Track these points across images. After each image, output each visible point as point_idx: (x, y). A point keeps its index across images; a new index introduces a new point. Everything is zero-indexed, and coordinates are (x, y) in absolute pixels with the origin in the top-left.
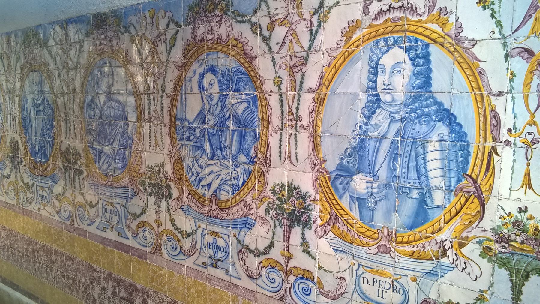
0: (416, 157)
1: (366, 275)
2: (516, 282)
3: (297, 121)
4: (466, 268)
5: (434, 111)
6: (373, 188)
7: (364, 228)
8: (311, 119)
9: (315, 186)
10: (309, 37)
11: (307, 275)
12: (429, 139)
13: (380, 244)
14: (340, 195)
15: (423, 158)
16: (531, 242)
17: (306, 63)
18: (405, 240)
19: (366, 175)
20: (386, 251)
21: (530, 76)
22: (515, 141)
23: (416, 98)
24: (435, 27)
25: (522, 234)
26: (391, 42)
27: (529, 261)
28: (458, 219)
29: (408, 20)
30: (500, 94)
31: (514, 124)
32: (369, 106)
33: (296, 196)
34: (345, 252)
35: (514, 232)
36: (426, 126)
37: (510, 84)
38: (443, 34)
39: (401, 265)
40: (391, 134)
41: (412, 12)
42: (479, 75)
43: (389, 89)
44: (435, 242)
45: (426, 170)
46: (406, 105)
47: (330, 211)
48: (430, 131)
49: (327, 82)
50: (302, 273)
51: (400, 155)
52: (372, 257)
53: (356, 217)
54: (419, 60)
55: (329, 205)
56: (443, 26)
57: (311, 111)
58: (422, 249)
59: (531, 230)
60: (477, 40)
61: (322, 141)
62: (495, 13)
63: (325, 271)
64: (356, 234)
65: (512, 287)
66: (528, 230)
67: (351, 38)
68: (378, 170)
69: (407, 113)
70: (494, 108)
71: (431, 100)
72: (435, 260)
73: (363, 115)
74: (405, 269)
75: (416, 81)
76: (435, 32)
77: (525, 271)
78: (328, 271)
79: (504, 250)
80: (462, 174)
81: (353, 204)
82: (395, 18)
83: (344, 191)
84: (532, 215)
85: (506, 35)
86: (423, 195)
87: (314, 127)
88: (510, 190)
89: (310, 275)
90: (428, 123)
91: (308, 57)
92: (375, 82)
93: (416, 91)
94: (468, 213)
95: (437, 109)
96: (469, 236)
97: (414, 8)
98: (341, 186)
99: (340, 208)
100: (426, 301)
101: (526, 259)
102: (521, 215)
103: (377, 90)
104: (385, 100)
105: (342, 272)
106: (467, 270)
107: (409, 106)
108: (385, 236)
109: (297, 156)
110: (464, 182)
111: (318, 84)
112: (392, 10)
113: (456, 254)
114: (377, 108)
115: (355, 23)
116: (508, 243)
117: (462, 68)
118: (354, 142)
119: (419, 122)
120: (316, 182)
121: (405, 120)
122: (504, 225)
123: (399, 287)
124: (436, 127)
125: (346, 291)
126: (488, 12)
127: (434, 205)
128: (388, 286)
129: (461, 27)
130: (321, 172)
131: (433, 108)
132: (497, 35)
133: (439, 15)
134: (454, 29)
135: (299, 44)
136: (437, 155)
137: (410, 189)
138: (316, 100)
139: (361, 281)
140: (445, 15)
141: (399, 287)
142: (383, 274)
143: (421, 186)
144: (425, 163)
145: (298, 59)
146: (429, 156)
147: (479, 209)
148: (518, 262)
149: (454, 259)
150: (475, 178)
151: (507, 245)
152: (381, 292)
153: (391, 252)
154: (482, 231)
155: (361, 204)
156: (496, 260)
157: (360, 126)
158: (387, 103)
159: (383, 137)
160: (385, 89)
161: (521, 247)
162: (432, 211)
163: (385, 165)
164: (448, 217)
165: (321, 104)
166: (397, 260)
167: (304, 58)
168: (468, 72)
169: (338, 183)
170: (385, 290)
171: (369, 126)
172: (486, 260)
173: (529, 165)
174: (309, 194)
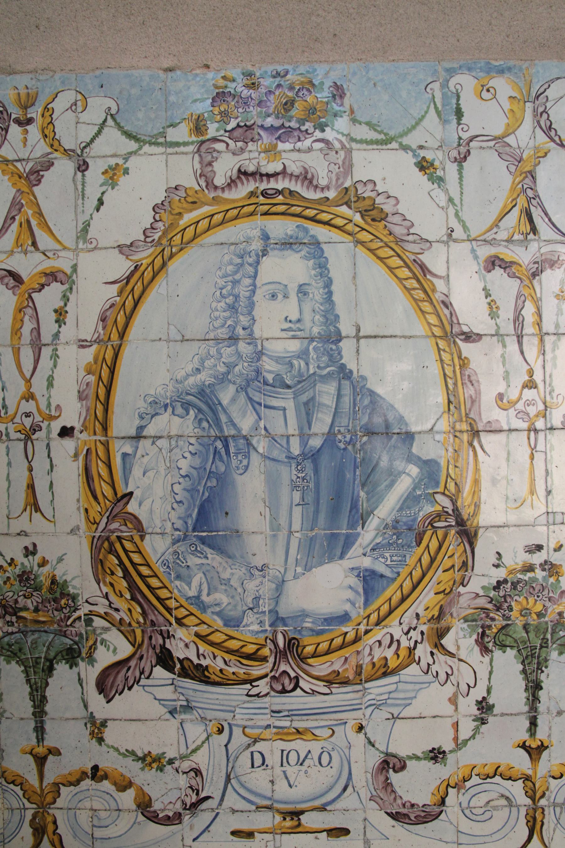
2: (36, 683)
16: (48, 605)
22: (6, 429)
25: (34, 594)
27: (50, 640)
35: (20, 594)
59: (47, 584)
65: (31, 694)
77: (46, 659)
79: (10, 629)
84: (44, 558)
88: (8, 518)
101: (44, 636)
102: (29, 560)
116: (15, 614)
122: (5, 583)
148: (34, 646)
151: (14, 619)
161: (35, 618)
173: (31, 470)
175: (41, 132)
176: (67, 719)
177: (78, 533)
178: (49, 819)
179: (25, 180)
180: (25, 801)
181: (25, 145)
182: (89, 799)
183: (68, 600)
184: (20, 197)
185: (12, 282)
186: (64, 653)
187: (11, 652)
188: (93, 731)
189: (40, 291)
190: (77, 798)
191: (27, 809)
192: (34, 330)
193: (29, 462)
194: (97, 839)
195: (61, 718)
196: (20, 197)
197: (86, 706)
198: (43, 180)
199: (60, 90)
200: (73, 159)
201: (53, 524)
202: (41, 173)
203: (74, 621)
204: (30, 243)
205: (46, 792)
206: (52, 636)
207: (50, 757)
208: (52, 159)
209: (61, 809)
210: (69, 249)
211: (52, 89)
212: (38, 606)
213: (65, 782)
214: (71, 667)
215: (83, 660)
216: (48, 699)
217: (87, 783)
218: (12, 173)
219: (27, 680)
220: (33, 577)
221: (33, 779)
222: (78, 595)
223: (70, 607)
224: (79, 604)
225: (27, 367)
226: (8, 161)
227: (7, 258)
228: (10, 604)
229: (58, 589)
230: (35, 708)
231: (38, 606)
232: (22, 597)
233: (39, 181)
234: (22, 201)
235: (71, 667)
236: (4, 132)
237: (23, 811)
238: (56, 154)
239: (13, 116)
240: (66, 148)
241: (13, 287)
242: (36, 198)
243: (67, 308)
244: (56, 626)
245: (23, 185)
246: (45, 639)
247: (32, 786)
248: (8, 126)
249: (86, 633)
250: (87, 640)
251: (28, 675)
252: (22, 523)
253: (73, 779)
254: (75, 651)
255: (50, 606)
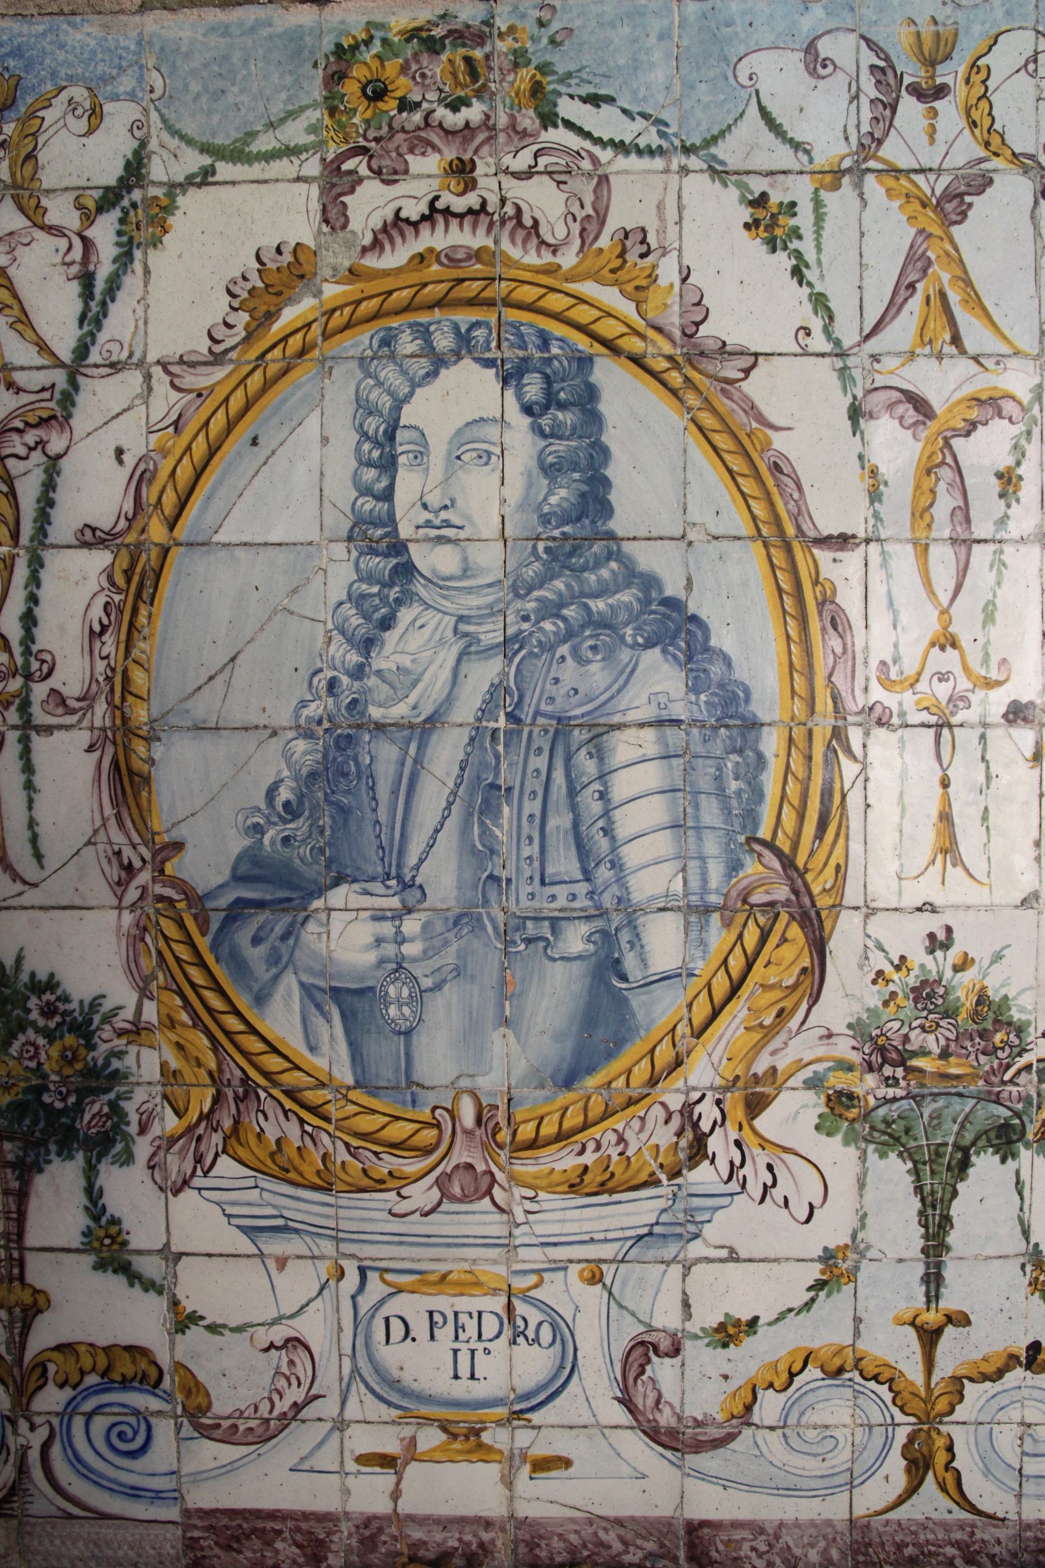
0: (572, 792)
1: (396, 1306)
2: (933, 1192)
3: (28, 677)
4: (774, 1185)
5: (628, 607)
6: (404, 941)
7: (374, 1112)
8: (100, 666)
9: (132, 967)
10: (78, 306)
11: (125, 1367)
12: (616, 719)
13: (447, 1166)
14: (256, 987)
15: (596, 795)
16: (968, 1044)
17: (68, 417)
18: (549, 1129)
19: (370, 886)
20: (476, 1190)
21: (928, 482)
22: (900, 704)
23: (555, 559)
24: (610, 297)
25: (942, 1023)
26: (443, 342)
27: (967, 1109)
28: (738, 1012)
29: (509, 262)
30: (843, 541)
31: (896, 646)
32: (363, 596)
33: (41, 1022)
34: (297, 1231)
35: (915, 1024)
36: (603, 669)
37: (871, 511)
38: (640, 324)
39: (539, 1229)
40: (466, 710)
41: (520, 234)
42: (772, 474)
43: (447, 524)
44: (662, 1114)
45: (613, 839)
46: (520, 590)
47: (213, 1065)
48: (616, 686)
49: (170, 499)
50: (102, 1362)
51: (509, 789)
52: (416, 1225)
53: (336, 1073)
54: (560, 415)
55: (206, 1042)
56: (639, 294)
57: (97, 628)
58: (614, 1152)
59: (968, 1004)
60: (756, 355)
61: (157, 756)
62: (807, 266)
63: (214, 1329)
64: (340, 1145)
65: (921, 1213)
66: (958, 1008)
67: (271, 316)
68: (421, 861)
69: (526, 618)
70: (829, 593)
71: (614, 565)
72: (665, 1182)
73: (343, 632)
74: (555, 1244)
75: (550, 492)
76: (610, 315)
77: (957, 1146)
78: (224, 1326)
79: (891, 1092)
80: (742, 839)
81: (318, 1021)
82: (455, 252)
83: (274, 971)
84: (966, 954)
85: (846, 343)
86: (607, 938)
87: (117, 700)
88: (900, 879)
89: (143, 1365)
90: (609, 658)
91: (76, 388)
92: (388, 495)
93: (556, 533)
94: (772, 981)
95: (639, 600)
96: (781, 1066)
97: (528, 222)
98: (262, 949)
99: (259, 1046)
100: (642, 1343)
101: (956, 1104)
102: (935, 959)
103: (396, 529)
104: (434, 571)
105: (292, 1316)
106: (778, 1193)
107: (531, 589)
108: (468, 1133)
109: (34, 839)
110: (752, 868)
111: (129, 506)
112: (440, 219)
113: (738, 1144)
114: (399, 602)
115: (287, 258)
116: (902, 1063)
117: (715, 448)
118: (306, 753)
119: (575, 652)
120: (141, 946)
121: (521, 648)
122: (886, 1004)
123: (534, 1316)
124: (641, 667)
125: (313, 1392)
126: (783, 261)
127: (651, 971)
128: (490, 1326)
129: (699, 304)
130: (160, 898)
131: (626, 597)
132: (819, 342)
133: (622, 254)
134: (676, 308)
135: (29, 334)
136: (651, 775)
137: (554, 923)
138: (120, 580)
139: (379, 1334)
140: (643, 256)
141: (534, 1316)
142: (472, 1285)
143: (598, 907)
144: (606, 814)
145: (25, 398)
146: (622, 785)
147: (806, 962)
148: (935, 1122)
149: (732, 1163)
150: (786, 849)
151: (900, 1072)
152: (464, 1358)
153: (496, 1187)
154: (821, 1038)
155: (354, 1014)
156: (870, 1134)
157: (332, 685)
158: (439, 582)
159: (433, 721)
160: (428, 524)
161: (942, 1070)
162: (644, 998)
163: (448, 838)
164: (701, 1011)
165: (145, 596)
166: (520, 1217)
167: (57, 396)
168: (737, 464)
169: (243, 936)
170: (480, 1346)
171: (372, 681)
172: (839, 1138)
173: (945, 784)
174: (107, 1005)
175: (964, 116)
176: (989, 1258)
177: (1035, 905)
178: (940, 1442)
179: (935, 210)
180: (895, 1411)
181: (932, 140)
182: (1019, 1405)
183: (1008, 1034)
184: (924, 246)
185: (912, 416)
186: (992, 1135)
187: (890, 1135)
188: (1037, 1279)
189: (968, 434)
190: (995, 1404)
191: (898, 1425)
192: (958, 512)
193: (944, 770)
194: (1028, 1477)
195: (976, 1257)
196: (924, 246)
197: (1026, 1233)
198: (970, 214)
199: (1003, 28)
200: (1031, 174)
201: (986, 889)
202: (968, 199)
203: (1018, 1072)
204: (947, 337)
205: (936, 1393)
206: (971, 1102)
207: (949, 1330)
208: (988, 171)
209: (964, 1423)
210: (1026, 356)
211: (987, 25)
212: (948, 1046)
213: (975, 1375)
214: (1003, 1161)
215: (1028, 1145)
216: (954, 1221)
217: (1017, 1375)
218: (907, 196)
219: (916, 1188)
220: (941, 991)
221: (913, 1371)
222: (1028, 1023)
223: (1011, 1047)
224: (1029, 1040)
225: (944, 584)
226: (900, 171)
227: (903, 365)
228: (894, 1043)
229: (990, 1014)
230: (928, 1240)
231: (948, 1046)
232: (918, 1030)
233: (964, 215)
234: (929, 254)
235: (1003, 1161)
236: (888, 112)
237: (890, 1429)
238: (996, 163)
239: (907, 80)
240: (1017, 151)
241: (915, 424)
242: (957, 249)
243: (1020, 471)
244: (981, 1083)
245: (930, 221)
246: (958, 1108)
247: (912, 1384)
248: (897, 100)
249: (1039, 1095)
250: (1039, 1108)
251: (918, 1179)
252: (927, 889)
253: (990, 1369)
254: (1014, 1132)
255: (973, 1046)
